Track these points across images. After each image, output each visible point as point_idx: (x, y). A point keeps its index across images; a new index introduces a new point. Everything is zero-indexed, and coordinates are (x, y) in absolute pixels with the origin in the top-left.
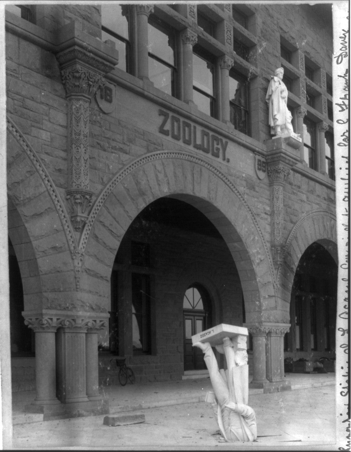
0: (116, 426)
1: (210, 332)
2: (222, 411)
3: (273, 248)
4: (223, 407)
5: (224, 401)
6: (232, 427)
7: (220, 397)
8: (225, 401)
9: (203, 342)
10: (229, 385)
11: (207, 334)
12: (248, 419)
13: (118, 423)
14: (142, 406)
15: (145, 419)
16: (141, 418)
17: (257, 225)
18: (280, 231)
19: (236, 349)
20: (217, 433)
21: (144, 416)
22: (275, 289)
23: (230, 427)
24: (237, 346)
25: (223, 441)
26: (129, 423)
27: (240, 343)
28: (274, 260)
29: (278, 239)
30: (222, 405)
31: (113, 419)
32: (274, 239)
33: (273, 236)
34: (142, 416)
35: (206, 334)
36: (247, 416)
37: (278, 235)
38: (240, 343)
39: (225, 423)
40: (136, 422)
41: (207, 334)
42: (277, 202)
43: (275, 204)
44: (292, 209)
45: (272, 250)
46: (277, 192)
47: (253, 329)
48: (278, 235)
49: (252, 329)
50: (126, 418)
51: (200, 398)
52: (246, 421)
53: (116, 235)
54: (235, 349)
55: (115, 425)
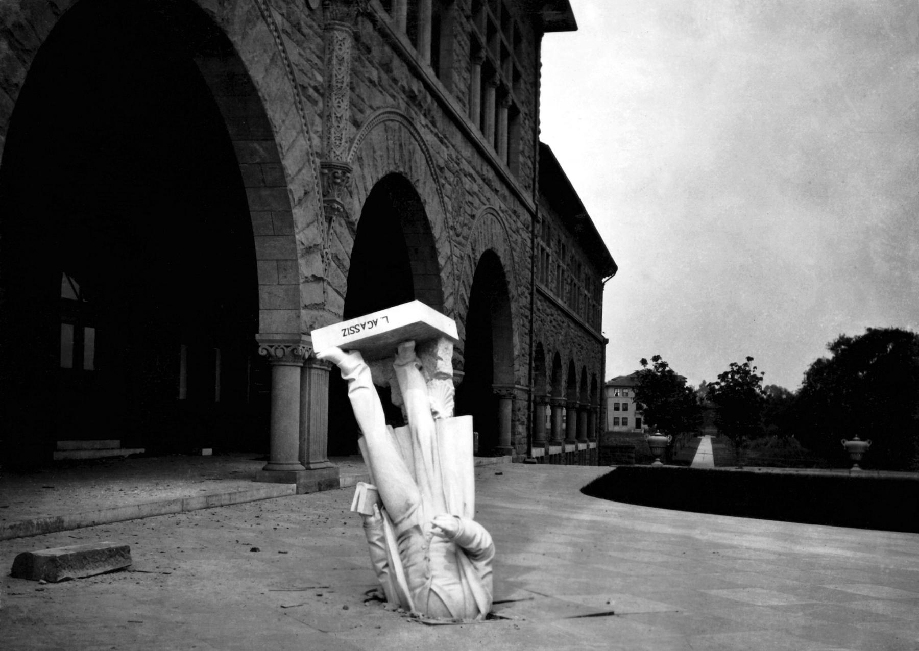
0: (61, 581)
1: (375, 323)
2: (402, 538)
3: (326, 171)
4: (405, 526)
5: (407, 509)
6: (435, 581)
7: (394, 499)
8: (411, 510)
9: (346, 349)
10: (420, 466)
11: (363, 326)
12: (477, 560)
13: (66, 574)
14: (63, 522)
15: (129, 558)
16: (123, 556)
17: (302, 110)
18: (342, 134)
19: (431, 374)
20: (371, 595)
21: (129, 551)
22: (325, 264)
23: (428, 582)
24: (435, 366)
25: (442, 621)
26: (92, 572)
27: (441, 359)
28: (325, 199)
29: (338, 153)
30: (401, 522)
31: (52, 560)
32: (329, 152)
33: (325, 143)
34: (124, 552)
35: (360, 328)
36: (481, 550)
37: (338, 143)
38: (441, 359)
39: (411, 569)
40: (109, 568)
41: (363, 326)
42: (340, 69)
43: (335, 72)
44: (357, 93)
45: (322, 174)
46: (340, 45)
47: (277, 348)
48: (338, 143)
49: (274, 348)
50: (85, 558)
51: (185, 501)
52: (476, 563)
53: (19, 47)
54: (427, 374)
55: (59, 579)
